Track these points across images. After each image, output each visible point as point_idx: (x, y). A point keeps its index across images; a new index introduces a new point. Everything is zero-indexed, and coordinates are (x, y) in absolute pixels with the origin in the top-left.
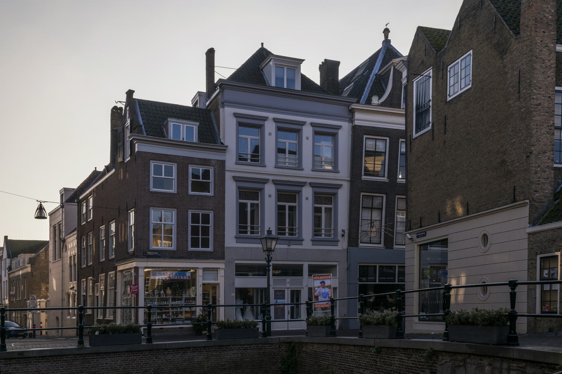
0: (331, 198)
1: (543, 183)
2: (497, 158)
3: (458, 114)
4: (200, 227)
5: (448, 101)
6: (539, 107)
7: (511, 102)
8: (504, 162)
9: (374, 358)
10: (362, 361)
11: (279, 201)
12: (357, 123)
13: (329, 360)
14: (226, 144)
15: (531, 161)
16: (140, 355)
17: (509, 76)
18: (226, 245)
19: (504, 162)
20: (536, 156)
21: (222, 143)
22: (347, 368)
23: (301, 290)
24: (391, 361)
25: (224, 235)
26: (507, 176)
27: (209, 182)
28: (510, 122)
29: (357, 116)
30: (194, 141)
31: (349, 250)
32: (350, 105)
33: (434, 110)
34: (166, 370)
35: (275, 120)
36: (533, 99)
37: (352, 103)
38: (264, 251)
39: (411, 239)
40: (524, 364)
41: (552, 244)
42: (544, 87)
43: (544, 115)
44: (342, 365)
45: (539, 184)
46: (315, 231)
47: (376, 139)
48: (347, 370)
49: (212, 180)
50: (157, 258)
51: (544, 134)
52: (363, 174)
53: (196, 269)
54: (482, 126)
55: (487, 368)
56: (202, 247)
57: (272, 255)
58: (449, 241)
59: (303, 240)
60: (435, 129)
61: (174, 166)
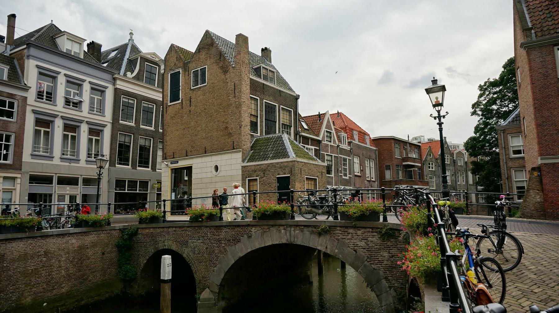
2: (223, 125)
4: (3, 145)
6: (244, 103)
11: (36, 126)
12: (118, 87)
14: (29, 85)
17: (229, 84)
18: (24, 160)
19: (227, 127)
21: (25, 84)
25: (22, 152)
27: (13, 111)
29: (118, 82)
30: (4, 79)
35: (90, 83)
39: (167, 165)
40: (303, 227)
46: (89, 154)
47: (129, 99)
49: (15, 110)
50: (7, 169)
55: (283, 231)
56: (3, 160)
58: (193, 168)
59: (53, 157)
60: (183, 102)
61: (15, 102)
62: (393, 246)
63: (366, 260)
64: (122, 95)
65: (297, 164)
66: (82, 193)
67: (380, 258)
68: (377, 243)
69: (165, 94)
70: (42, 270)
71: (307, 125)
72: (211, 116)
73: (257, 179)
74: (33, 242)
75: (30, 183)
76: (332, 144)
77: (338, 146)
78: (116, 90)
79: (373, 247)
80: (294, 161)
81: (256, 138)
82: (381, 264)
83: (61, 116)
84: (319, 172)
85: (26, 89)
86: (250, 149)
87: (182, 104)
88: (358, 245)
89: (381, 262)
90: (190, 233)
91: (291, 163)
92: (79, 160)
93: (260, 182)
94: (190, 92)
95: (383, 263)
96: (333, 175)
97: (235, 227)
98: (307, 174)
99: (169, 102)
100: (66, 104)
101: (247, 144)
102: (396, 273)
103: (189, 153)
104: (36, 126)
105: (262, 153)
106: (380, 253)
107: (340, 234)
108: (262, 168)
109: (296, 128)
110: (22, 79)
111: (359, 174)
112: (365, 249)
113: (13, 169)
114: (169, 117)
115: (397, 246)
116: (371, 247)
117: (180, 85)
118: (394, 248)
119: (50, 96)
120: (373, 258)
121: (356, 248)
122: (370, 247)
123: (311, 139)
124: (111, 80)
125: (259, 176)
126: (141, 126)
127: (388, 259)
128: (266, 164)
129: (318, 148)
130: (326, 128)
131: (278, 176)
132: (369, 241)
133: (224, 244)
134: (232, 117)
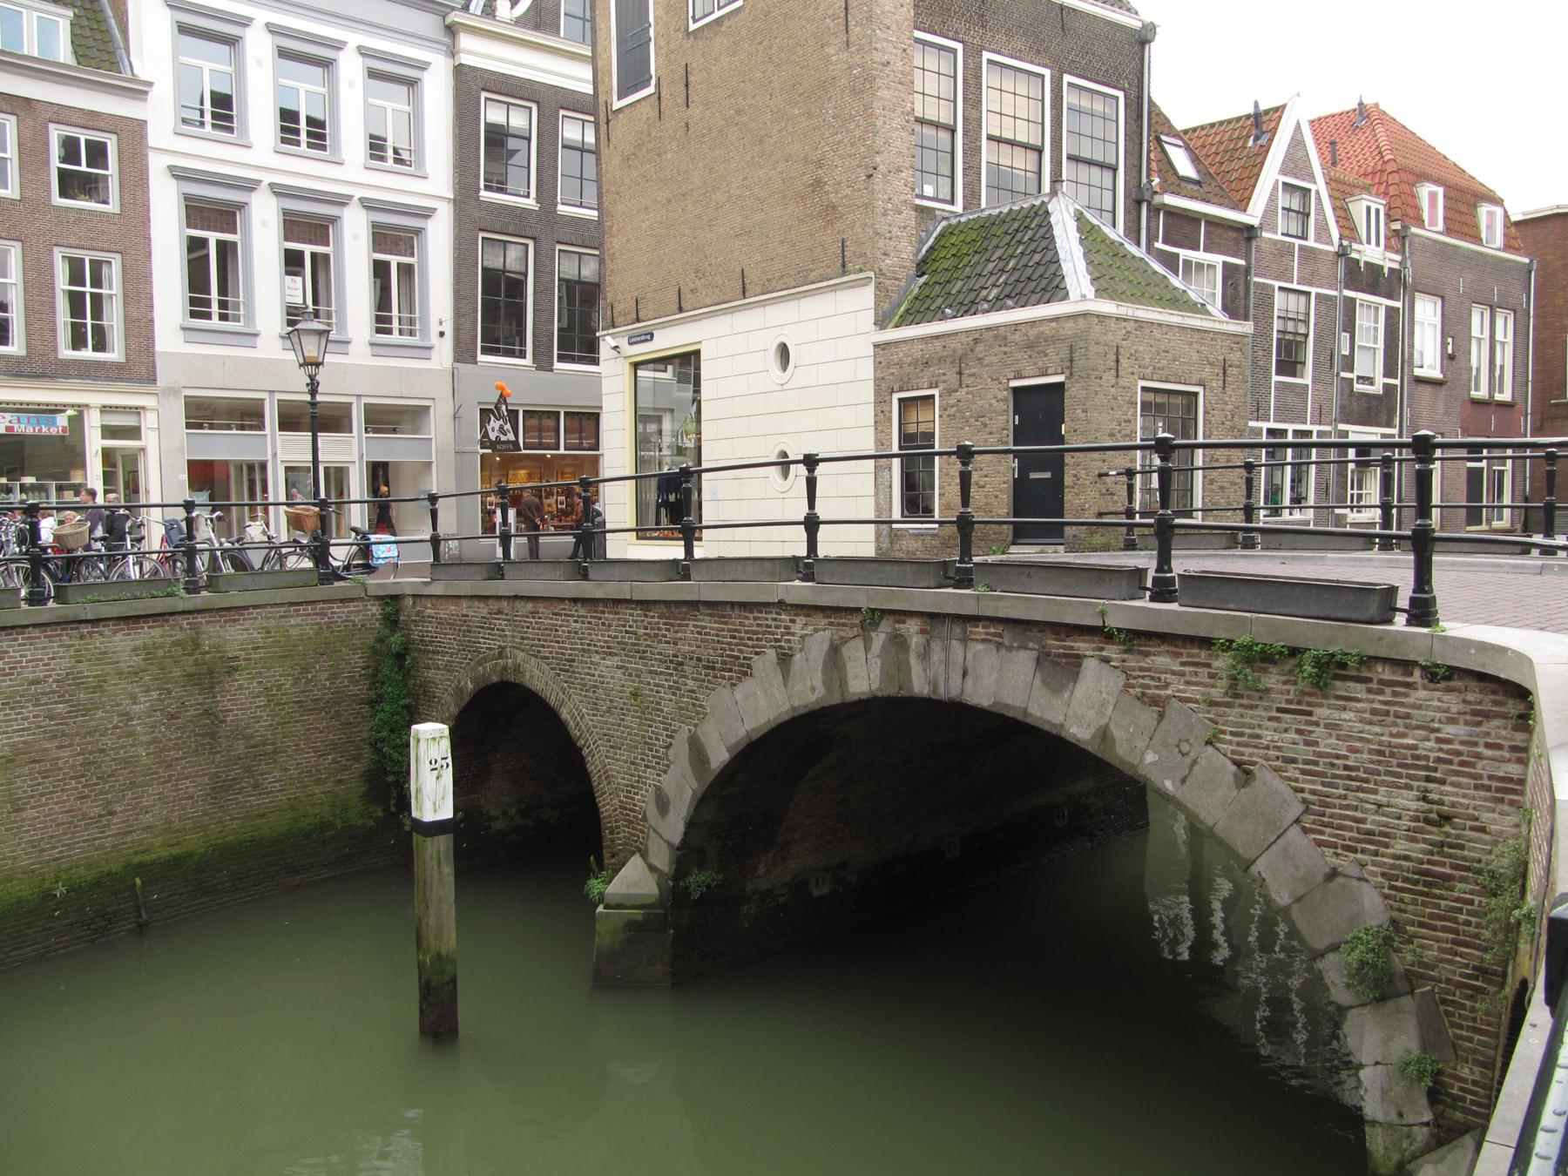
0: (412, 238)
1: (897, 237)
3: (715, 65)
5: (690, 30)
7: (831, 51)
8: (818, 184)
9: (631, 626)
10: (597, 635)
12: (466, 59)
13: (506, 636)
15: (875, 187)
16: (16, 640)
18: (160, 347)
19: (818, 184)
20: (885, 176)
22: (557, 653)
23: (348, 468)
24: (677, 632)
25: (152, 321)
26: (827, 215)
28: (829, 94)
29: (465, 41)
31: (456, 371)
32: (447, 14)
33: (661, 48)
34: (88, 677)
35: (363, 52)
36: (876, 49)
37: (453, 9)
38: (301, 365)
39: (616, 348)
41: (922, 371)
42: (894, 27)
43: (896, 89)
44: (543, 646)
45: (890, 239)
46: (379, 319)
48: (557, 659)
51: (897, 129)
52: (482, 186)
53: (81, 409)
54: (769, 97)
57: (322, 375)
62: (1450, 762)
63: (1297, 821)
64: (484, 89)
65: (1097, 329)
66: (365, 459)
67: (1371, 818)
68: (1361, 739)
69: (600, 64)
70: (58, 748)
71: (1195, 160)
72: (761, 141)
73: (932, 397)
74: (9, 646)
75: (189, 426)
76: (1311, 243)
77: (1342, 253)
78: (459, 70)
79: (1338, 757)
80: (1085, 315)
81: (944, 223)
82: (1376, 854)
83: (359, 199)
84: (1211, 364)
85: (139, 91)
86: (912, 272)
87: (659, 98)
88: (1258, 737)
89: (1371, 842)
90: (579, 625)
91: (1070, 324)
92: (256, 335)
93: (943, 409)
94: (687, 44)
95: (1387, 846)
96: (1307, 380)
97: (733, 609)
98: (1149, 371)
99: (615, 97)
100: (284, 141)
101: (903, 252)
102: (1452, 909)
103: (688, 298)
104: (286, 239)
105: (960, 284)
106: (1375, 792)
107: (1173, 673)
108: (954, 351)
109: (1135, 174)
110: (124, 56)
111: (1436, 374)
112: (1294, 761)
113: (130, 380)
114: (616, 161)
115: (1472, 765)
116: (1329, 755)
117: (651, 20)
118: (1457, 773)
119: (223, 108)
120: (1332, 816)
121: (1247, 750)
122: (1320, 755)
123: (1207, 223)
124: (440, 35)
125: (942, 386)
126: (562, 209)
127: (1416, 830)
128: (968, 332)
129: (1242, 262)
130: (1283, 172)
131: (1014, 383)
132: (1317, 724)
133: (693, 679)
134: (838, 137)
